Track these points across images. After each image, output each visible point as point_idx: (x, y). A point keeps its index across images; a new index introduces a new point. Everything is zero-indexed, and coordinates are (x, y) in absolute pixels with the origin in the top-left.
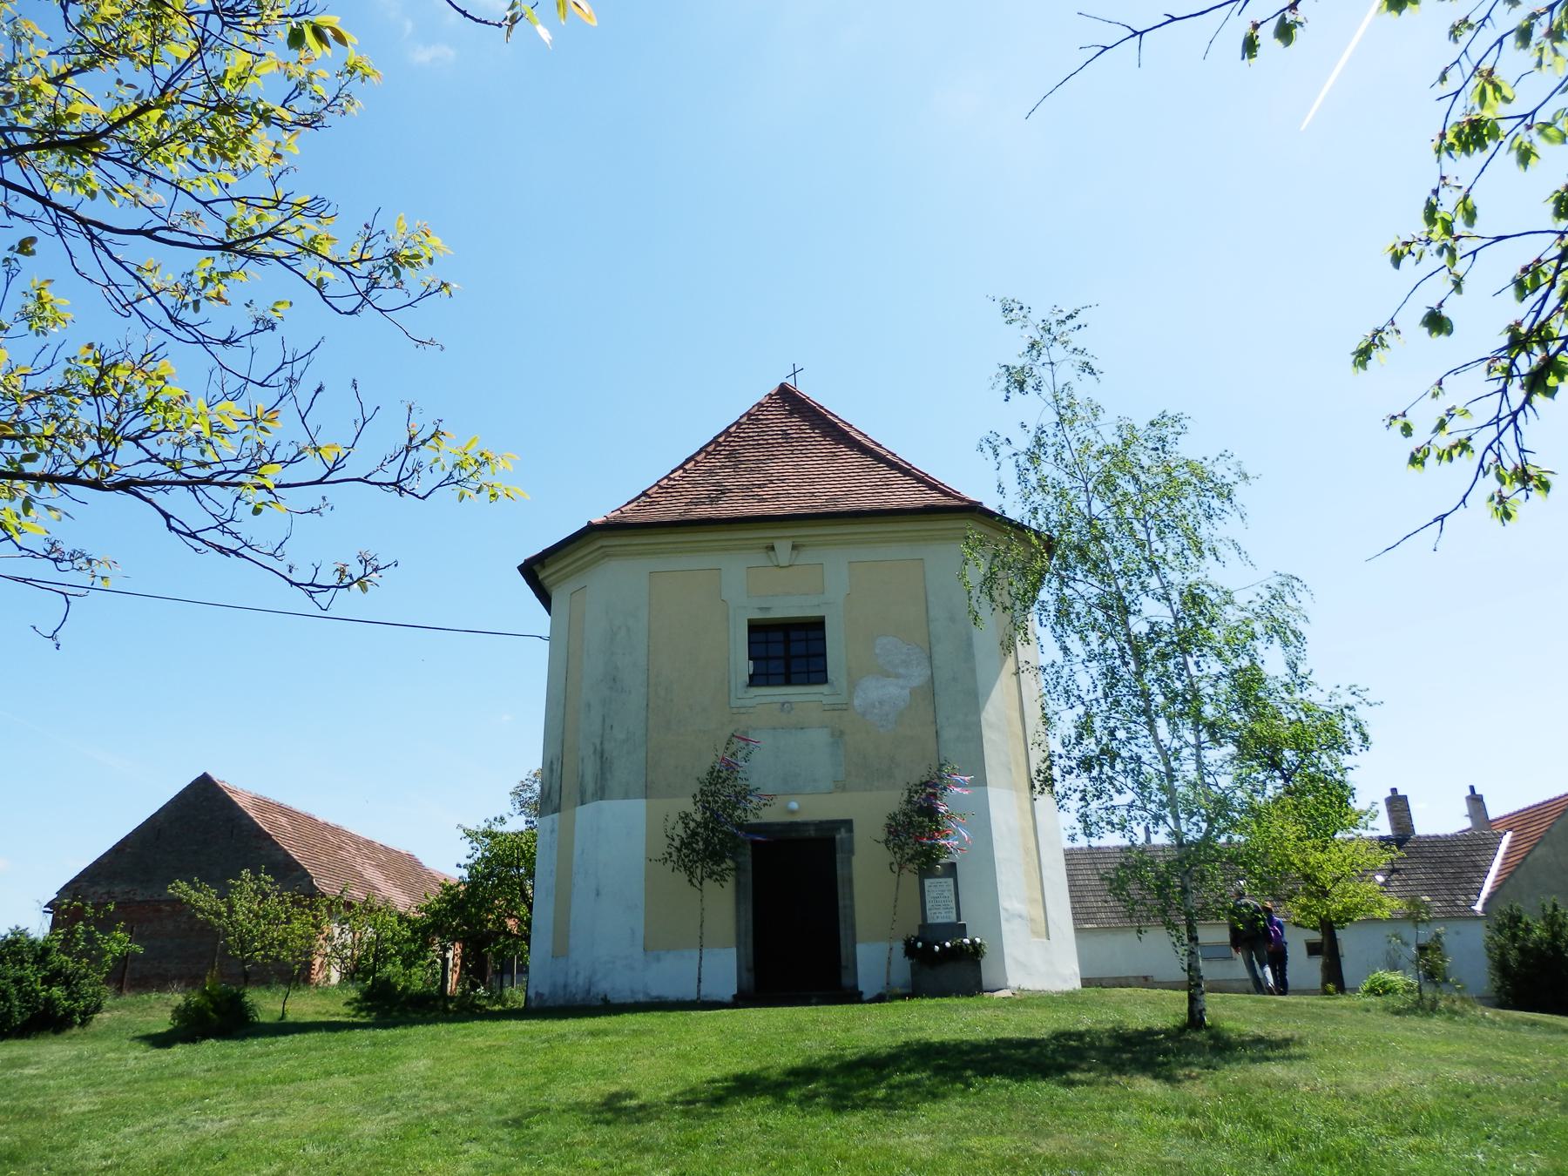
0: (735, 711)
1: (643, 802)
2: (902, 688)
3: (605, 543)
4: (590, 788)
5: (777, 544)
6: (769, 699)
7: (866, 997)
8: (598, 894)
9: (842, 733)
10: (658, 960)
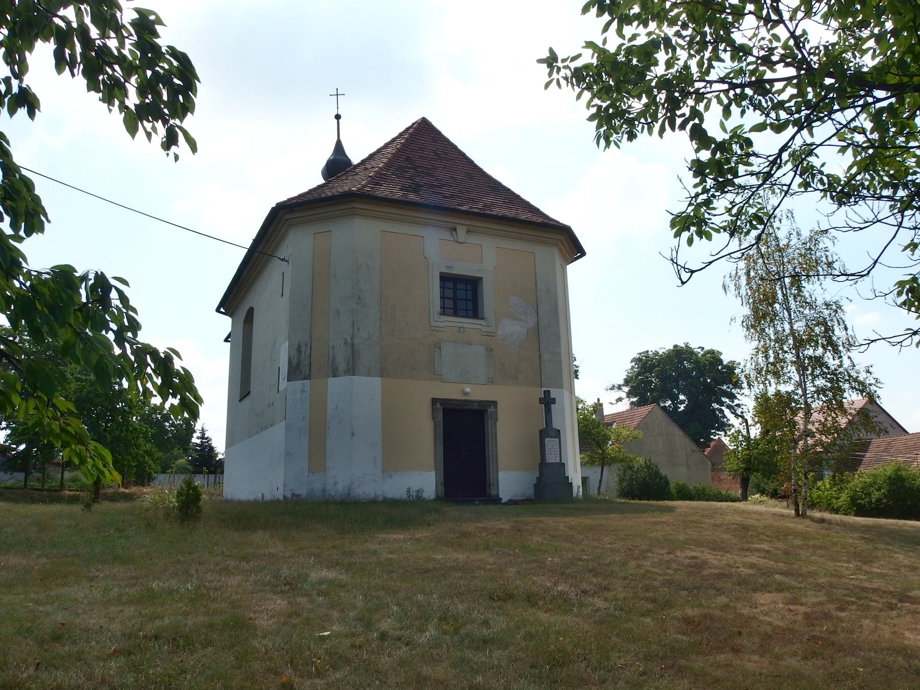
0: (432, 328)
1: (377, 381)
2: (523, 328)
3: (358, 206)
4: (342, 366)
5: (459, 228)
6: (452, 324)
7: (503, 501)
8: (353, 435)
9: (491, 350)
10: (391, 477)
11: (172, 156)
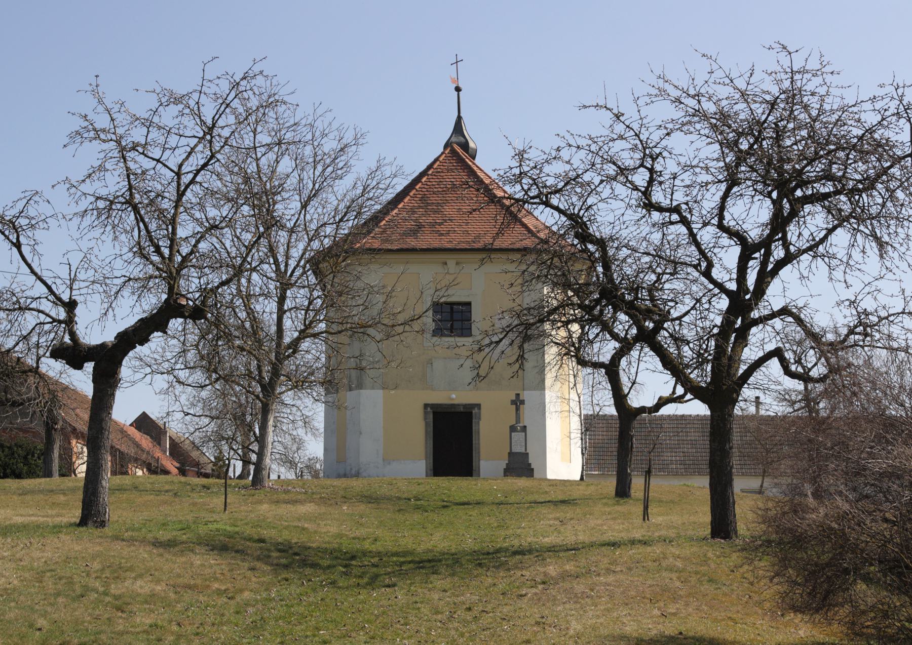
10: (389, 464)
11: (775, 45)
